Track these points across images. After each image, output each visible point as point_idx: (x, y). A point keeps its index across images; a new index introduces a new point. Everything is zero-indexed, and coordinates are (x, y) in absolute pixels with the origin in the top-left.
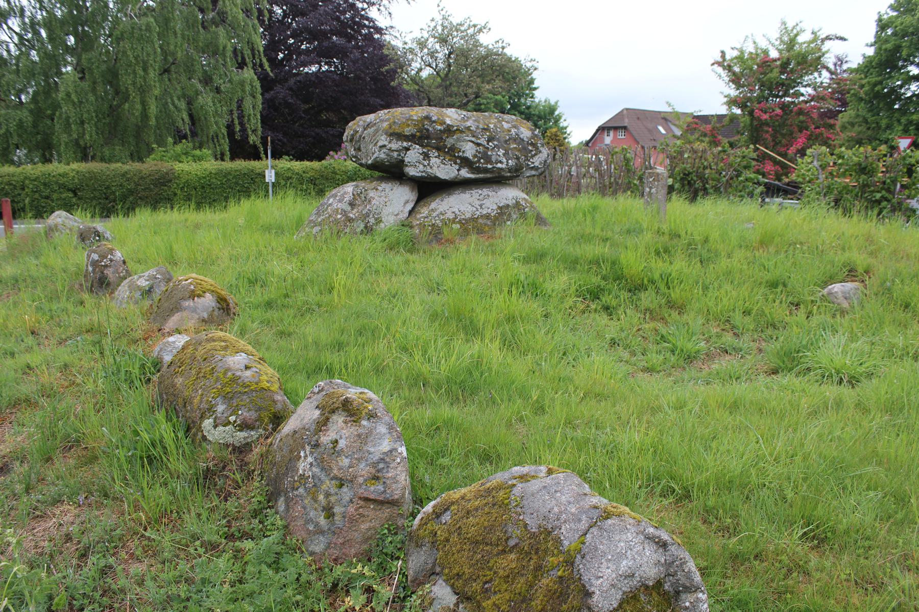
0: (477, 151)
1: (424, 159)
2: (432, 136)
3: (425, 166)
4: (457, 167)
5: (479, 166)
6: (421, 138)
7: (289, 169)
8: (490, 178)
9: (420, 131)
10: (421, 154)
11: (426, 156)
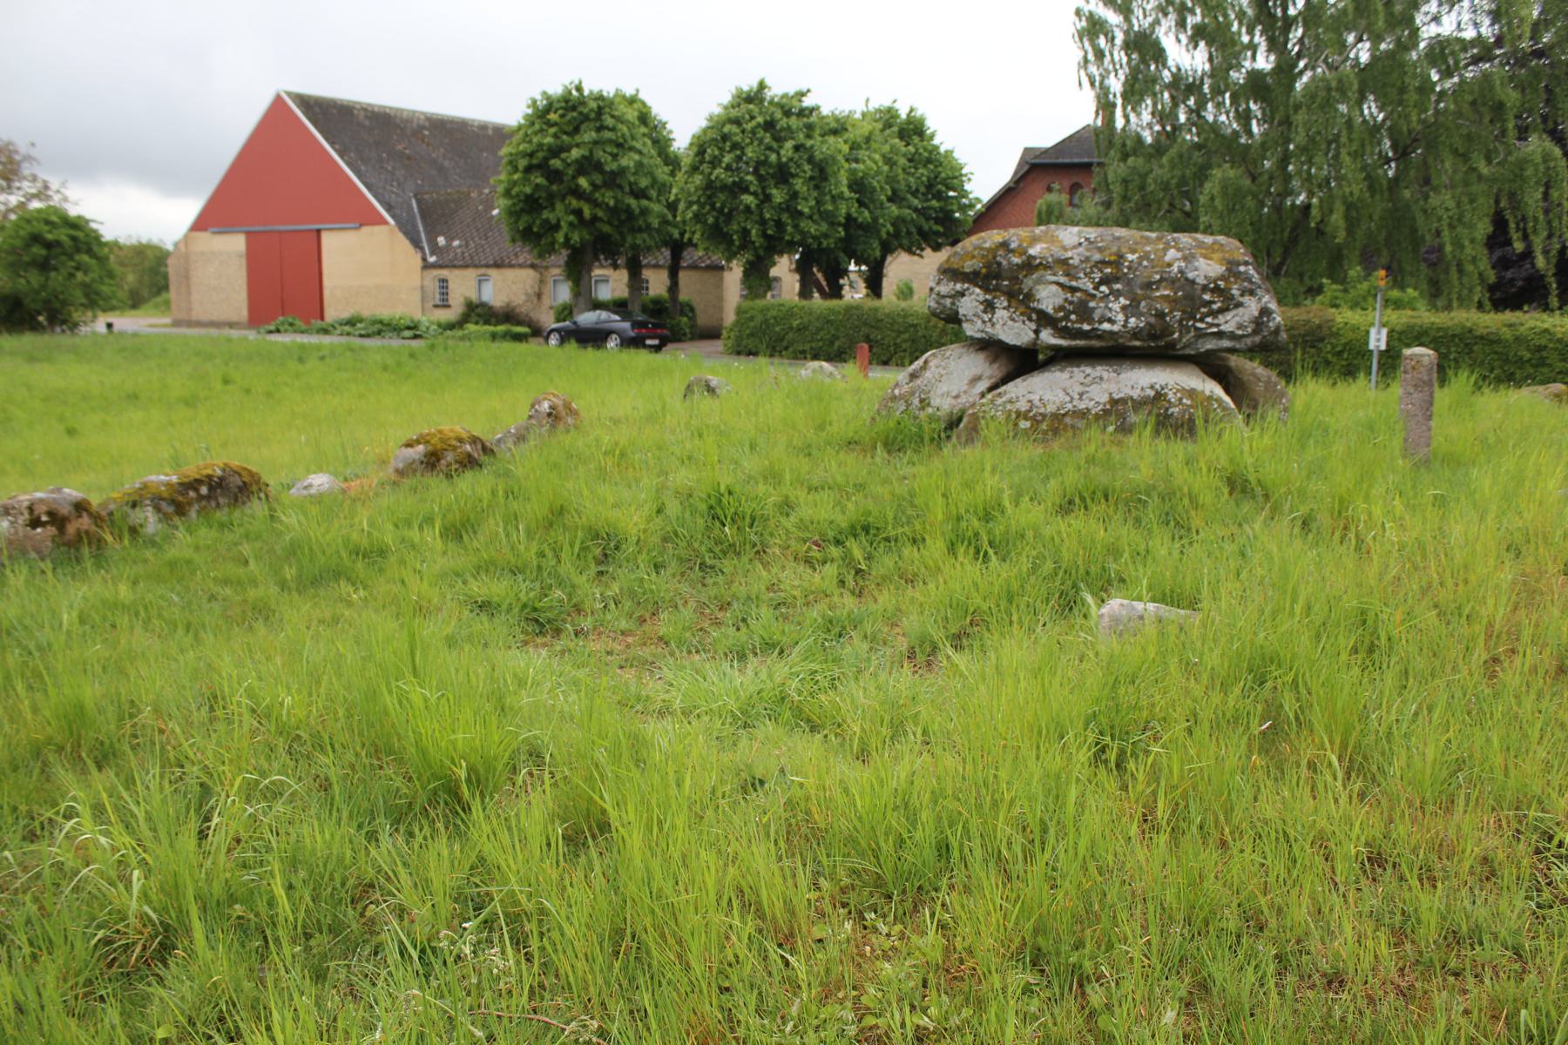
0: (1066, 300)
1: (985, 312)
2: (1004, 274)
3: (984, 322)
4: (1033, 326)
5: (1066, 327)
6: (988, 277)
7: (1546, 331)
8: (1102, 348)
9: (988, 266)
10: (981, 303)
11: (989, 307)
